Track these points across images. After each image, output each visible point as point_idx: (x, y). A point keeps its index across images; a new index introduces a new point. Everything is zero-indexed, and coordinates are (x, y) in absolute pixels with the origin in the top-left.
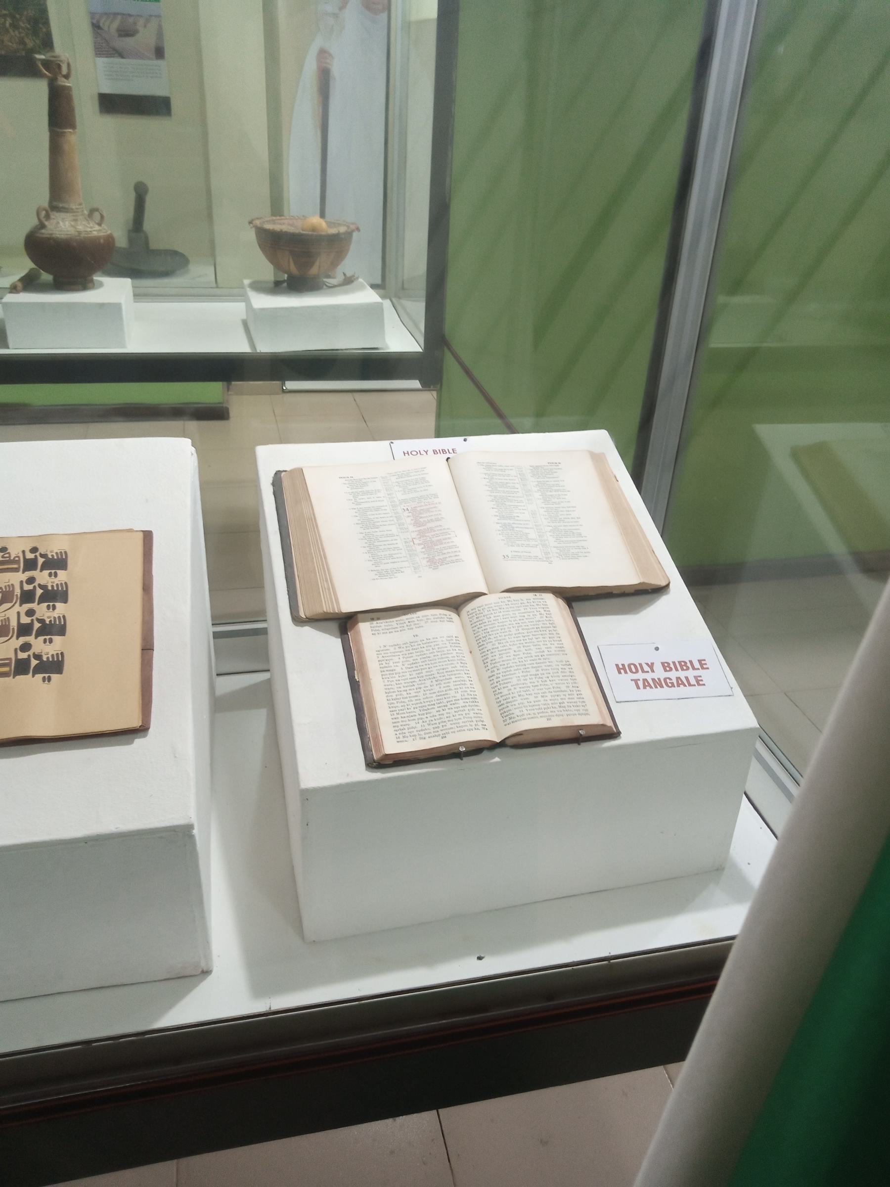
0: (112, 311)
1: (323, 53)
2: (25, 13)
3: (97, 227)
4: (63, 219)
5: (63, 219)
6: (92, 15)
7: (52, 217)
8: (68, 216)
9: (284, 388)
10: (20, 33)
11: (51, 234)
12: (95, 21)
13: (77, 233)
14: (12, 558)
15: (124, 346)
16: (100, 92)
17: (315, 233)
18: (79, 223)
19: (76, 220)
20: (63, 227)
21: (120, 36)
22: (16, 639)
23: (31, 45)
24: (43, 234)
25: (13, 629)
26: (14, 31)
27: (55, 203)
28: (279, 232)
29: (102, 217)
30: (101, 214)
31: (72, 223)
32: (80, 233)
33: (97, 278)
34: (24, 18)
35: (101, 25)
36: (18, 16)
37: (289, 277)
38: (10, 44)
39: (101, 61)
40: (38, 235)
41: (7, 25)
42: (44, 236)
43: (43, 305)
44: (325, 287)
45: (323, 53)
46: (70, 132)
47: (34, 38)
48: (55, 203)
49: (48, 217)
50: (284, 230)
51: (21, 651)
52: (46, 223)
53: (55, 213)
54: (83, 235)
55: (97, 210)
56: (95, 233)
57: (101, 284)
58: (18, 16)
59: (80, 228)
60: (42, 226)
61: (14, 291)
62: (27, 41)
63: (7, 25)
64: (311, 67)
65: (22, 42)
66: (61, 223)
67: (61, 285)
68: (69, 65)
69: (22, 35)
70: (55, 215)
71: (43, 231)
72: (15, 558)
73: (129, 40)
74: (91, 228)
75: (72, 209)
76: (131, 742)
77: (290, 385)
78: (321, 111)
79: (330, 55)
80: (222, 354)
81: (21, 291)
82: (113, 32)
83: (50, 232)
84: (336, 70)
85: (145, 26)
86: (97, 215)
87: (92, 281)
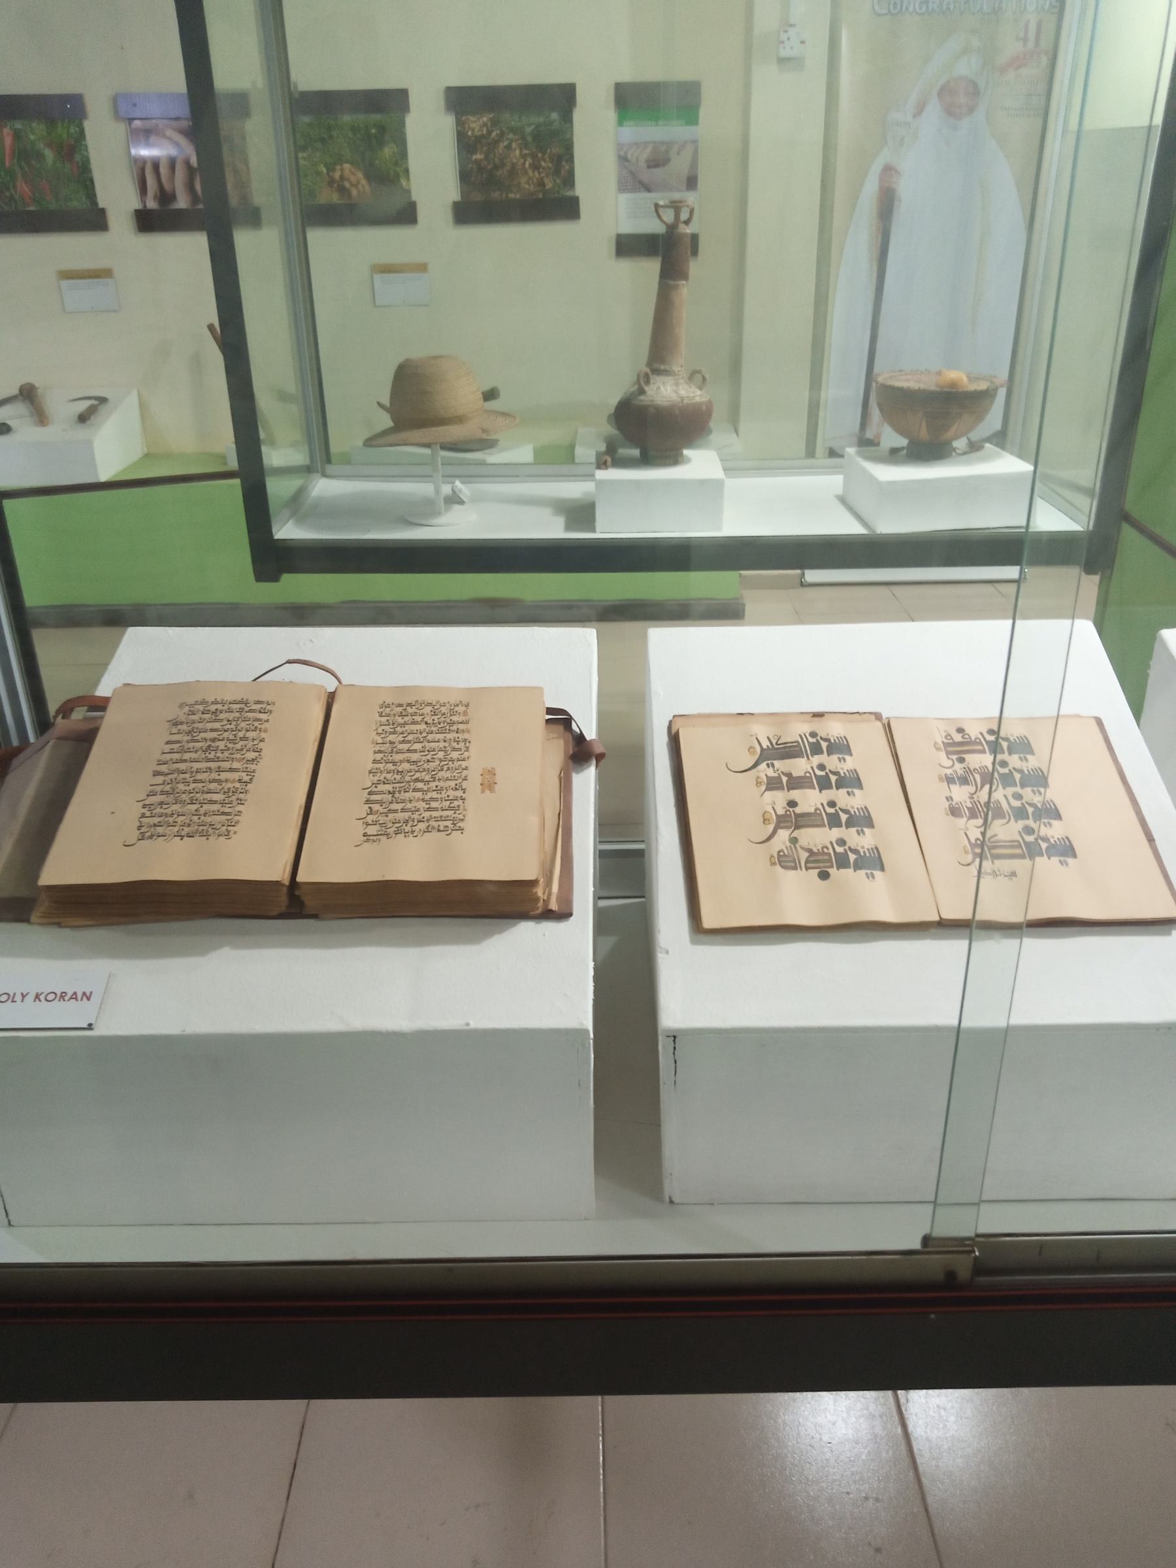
0: (710, 490)
1: (889, 170)
2: (549, 151)
3: (698, 392)
4: (664, 383)
5: (664, 383)
6: (620, 146)
7: (652, 381)
8: (669, 380)
9: (803, 580)
10: (539, 173)
11: (652, 401)
12: (622, 154)
13: (679, 400)
14: (973, 739)
15: (593, 530)
16: (619, 232)
17: (954, 390)
18: (681, 387)
19: (677, 384)
20: (665, 393)
21: (649, 167)
22: (1014, 822)
23: (551, 185)
24: (642, 401)
25: (1008, 812)
26: (533, 172)
27: (656, 366)
28: (916, 391)
29: (704, 379)
30: (703, 376)
31: (674, 388)
32: (682, 399)
33: (686, 452)
34: (546, 156)
35: (629, 157)
36: (540, 155)
37: (911, 442)
38: (527, 186)
39: (624, 198)
40: (637, 402)
41: (527, 165)
42: (644, 403)
43: (638, 483)
44: (954, 453)
45: (889, 170)
46: (683, 284)
47: (555, 177)
48: (656, 366)
49: (648, 382)
50: (921, 388)
51: (819, 872)
52: (646, 388)
53: (655, 377)
54: (685, 401)
55: (699, 372)
56: (698, 399)
57: (689, 460)
58: (540, 155)
59: (683, 393)
60: (642, 392)
61: (603, 467)
62: (546, 180)
63: (527, 165)
64: (871, 188)
65: (541, 184)
66: (662, 388)
67: (646, 460)
68: (692, 212)
69: (542, 175)
70: (654, 379)
71: (642, 398)
72: (976, 739)
73: (659, 172)
74: (693, 392)
75: (674, 372)
76: (1169, 934)
77: (812, 576)
78: (880, 240)
79: (897, 171)
80: (841, 537)
81: (610, 467)
82: (642, 164)
83: (651, 398)
84: (905, 189)
85: (678, 154)
86: (698, 377)
87: (682, 454)
